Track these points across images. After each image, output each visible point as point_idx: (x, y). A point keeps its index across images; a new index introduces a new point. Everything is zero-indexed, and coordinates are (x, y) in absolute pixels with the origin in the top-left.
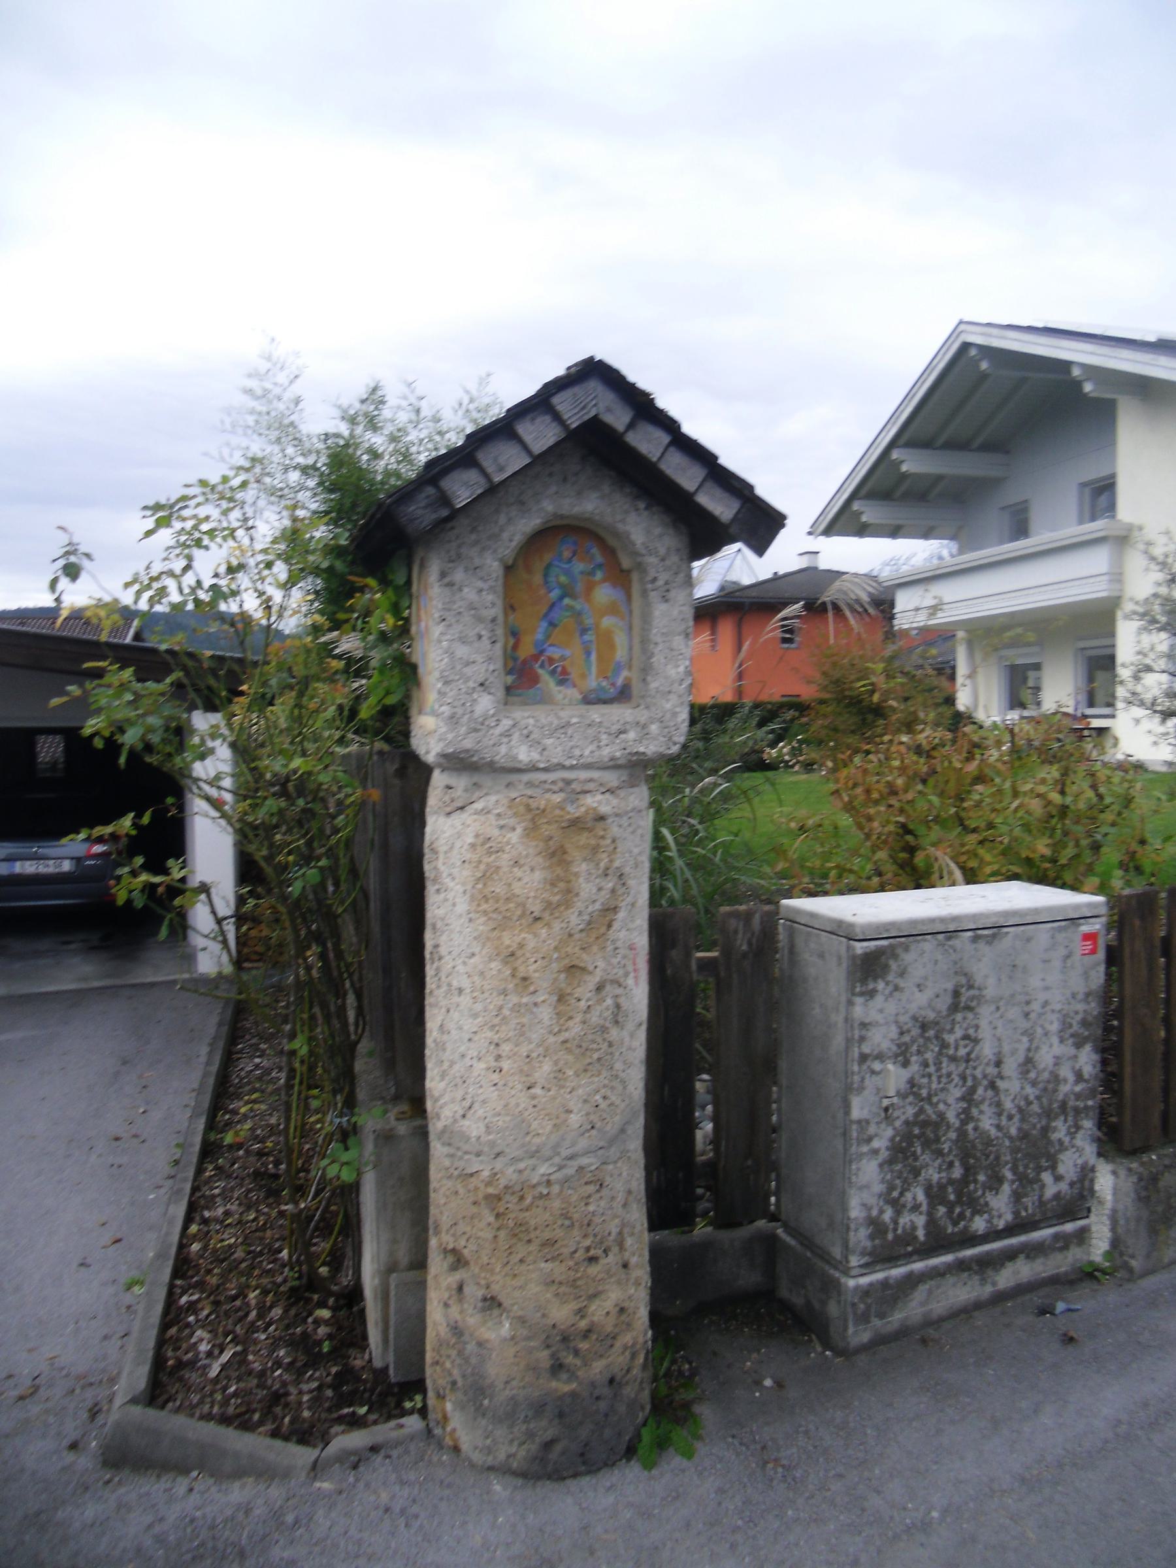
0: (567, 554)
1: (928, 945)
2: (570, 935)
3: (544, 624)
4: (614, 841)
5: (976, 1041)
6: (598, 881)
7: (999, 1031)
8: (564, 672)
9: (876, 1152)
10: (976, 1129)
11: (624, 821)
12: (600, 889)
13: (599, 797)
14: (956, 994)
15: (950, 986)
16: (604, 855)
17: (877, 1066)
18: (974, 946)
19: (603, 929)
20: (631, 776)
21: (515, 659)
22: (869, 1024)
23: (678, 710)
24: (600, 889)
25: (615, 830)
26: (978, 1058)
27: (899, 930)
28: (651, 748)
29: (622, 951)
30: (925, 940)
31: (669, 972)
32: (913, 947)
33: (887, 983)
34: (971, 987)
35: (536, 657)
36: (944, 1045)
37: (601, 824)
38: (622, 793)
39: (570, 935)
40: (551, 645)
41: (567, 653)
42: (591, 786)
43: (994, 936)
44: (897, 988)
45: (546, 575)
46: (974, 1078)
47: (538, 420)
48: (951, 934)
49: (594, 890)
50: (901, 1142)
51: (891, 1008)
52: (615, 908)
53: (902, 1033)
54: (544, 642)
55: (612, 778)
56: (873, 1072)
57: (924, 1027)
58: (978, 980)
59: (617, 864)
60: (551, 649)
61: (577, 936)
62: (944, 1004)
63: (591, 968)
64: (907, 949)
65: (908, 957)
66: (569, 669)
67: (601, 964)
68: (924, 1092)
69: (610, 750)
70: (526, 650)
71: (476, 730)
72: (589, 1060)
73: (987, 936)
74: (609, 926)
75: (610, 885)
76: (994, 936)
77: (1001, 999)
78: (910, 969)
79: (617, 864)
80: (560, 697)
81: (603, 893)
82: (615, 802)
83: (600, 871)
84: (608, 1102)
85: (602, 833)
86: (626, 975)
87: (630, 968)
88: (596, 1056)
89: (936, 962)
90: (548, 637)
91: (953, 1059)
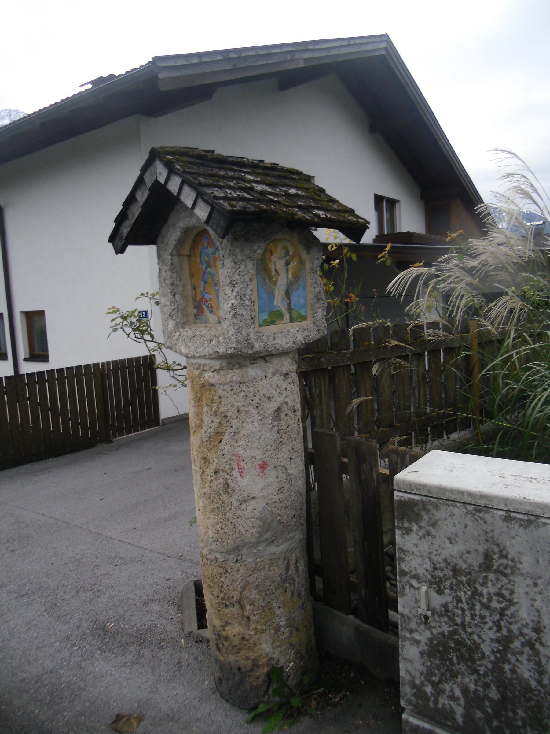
0: (206, 245)
1: (458, 511)
2: (203, 442)
3: (203, 282)
4: (220, 398)
5: (511, 603)
6: (211, 417)
7: (538, 604)
8: (211, 307)
9: (418, 642)
10: (513, 671)
11: (227, 387)
12: (212, 422)
13: (211, 374)
14: (487, 556)
15: (481, 549)
16: (216, 404)
17: (414, 583)
18: (506, 524)
19: (217, 443)
20: (228, 364)
21: (196, 301)
22: (406, 551)
23: (229, 328)
24: (212, 422)
25: (220, 392)
26: (513, 616)
27: (429, 491)
28: (221, 350)
29: (227, 456)
30: (455, 506)
31: (363, 477)
32: (443, 508)
33: (420, 528)
34: (502, 556)
35: (202, 300)
36: (476, 593)
37: (213, 389)
38: (222, 373)
39: (203, 442)
40: (206, 293)
41: (211, 297)
42: (207, 368)
43: (530, 522)
44: (428, 533)
45: (201, 257)
46: (510, 631)
47: (143, 188)
48: (480, 509)
49: (210, 422)
50: (438, 645)
51: (425, 546)
52: (223, 433)
53: (435, 568)
54: (204, 291)
55: (216, 364)
56: (411, 586)
57: (456, 571)
58: (512, 553)
59: (222, 410)
60: (207, 295)
61: (205, 443)
62: (476, 561)
63: (211, 461)
64: (437, 507)
65: (440, 514)
66: (213, 305)
67: (216, 461)
68: (459, 620)
69: (208, 351)
70: (199, 298)
71: (170, 337)
72: (213, 507)
73: (522, 520)
74: (220, 442)
75: (218, 420)
76: (530, 522)
77: (540, 578)
78: (440, 523)
79: (222, 410)
80: (211, 319)
81: (214, 424)
82: (218, 377)
83: (212, 413)
84: (223, 531)
85: (214, 393)
86: (233, 469)
87: (235, 466)
88: (216, 506)
89: (466, 526)
90: (204, 289)
91: (486, 606)
